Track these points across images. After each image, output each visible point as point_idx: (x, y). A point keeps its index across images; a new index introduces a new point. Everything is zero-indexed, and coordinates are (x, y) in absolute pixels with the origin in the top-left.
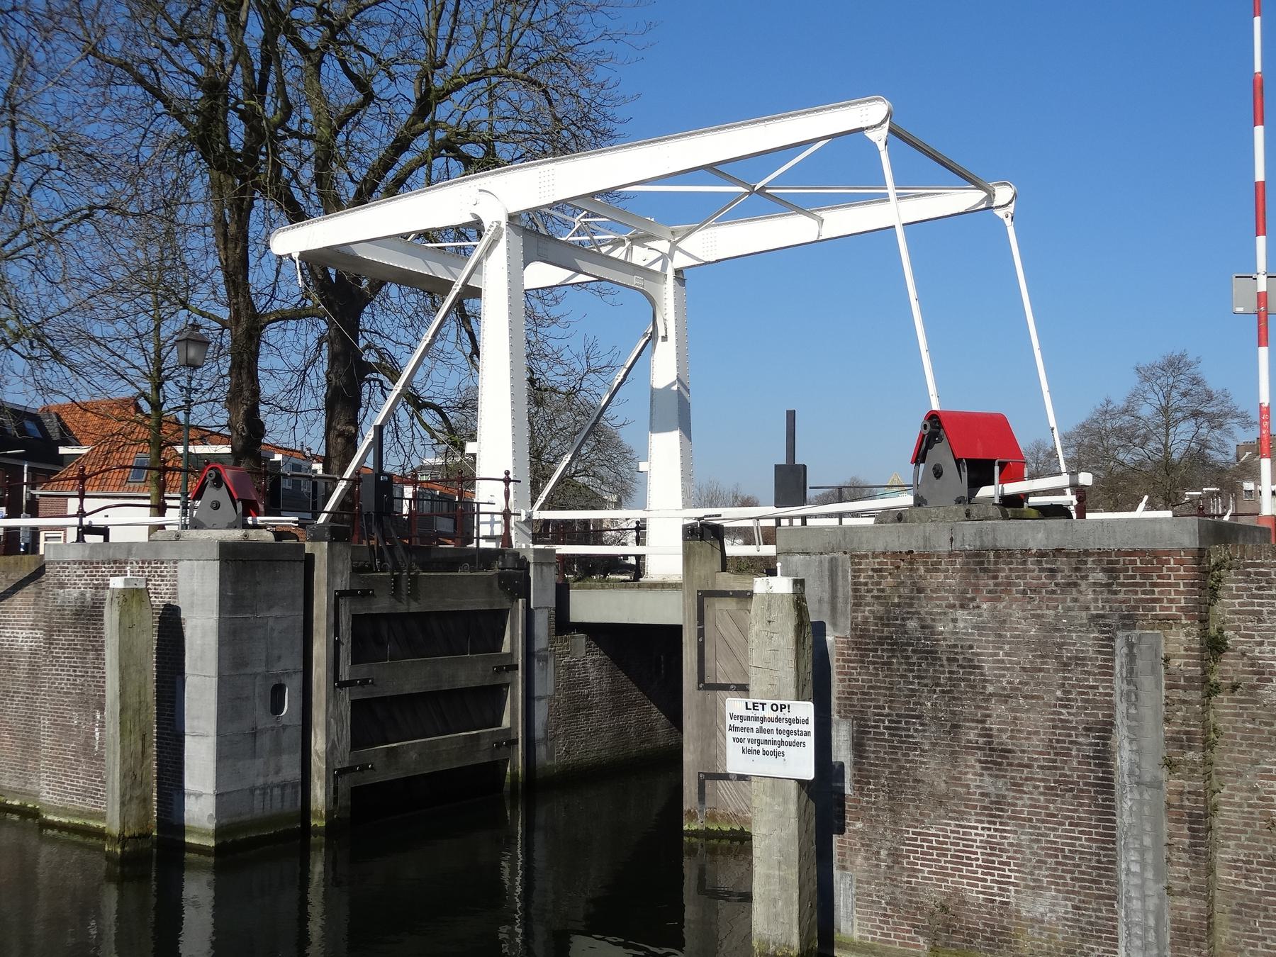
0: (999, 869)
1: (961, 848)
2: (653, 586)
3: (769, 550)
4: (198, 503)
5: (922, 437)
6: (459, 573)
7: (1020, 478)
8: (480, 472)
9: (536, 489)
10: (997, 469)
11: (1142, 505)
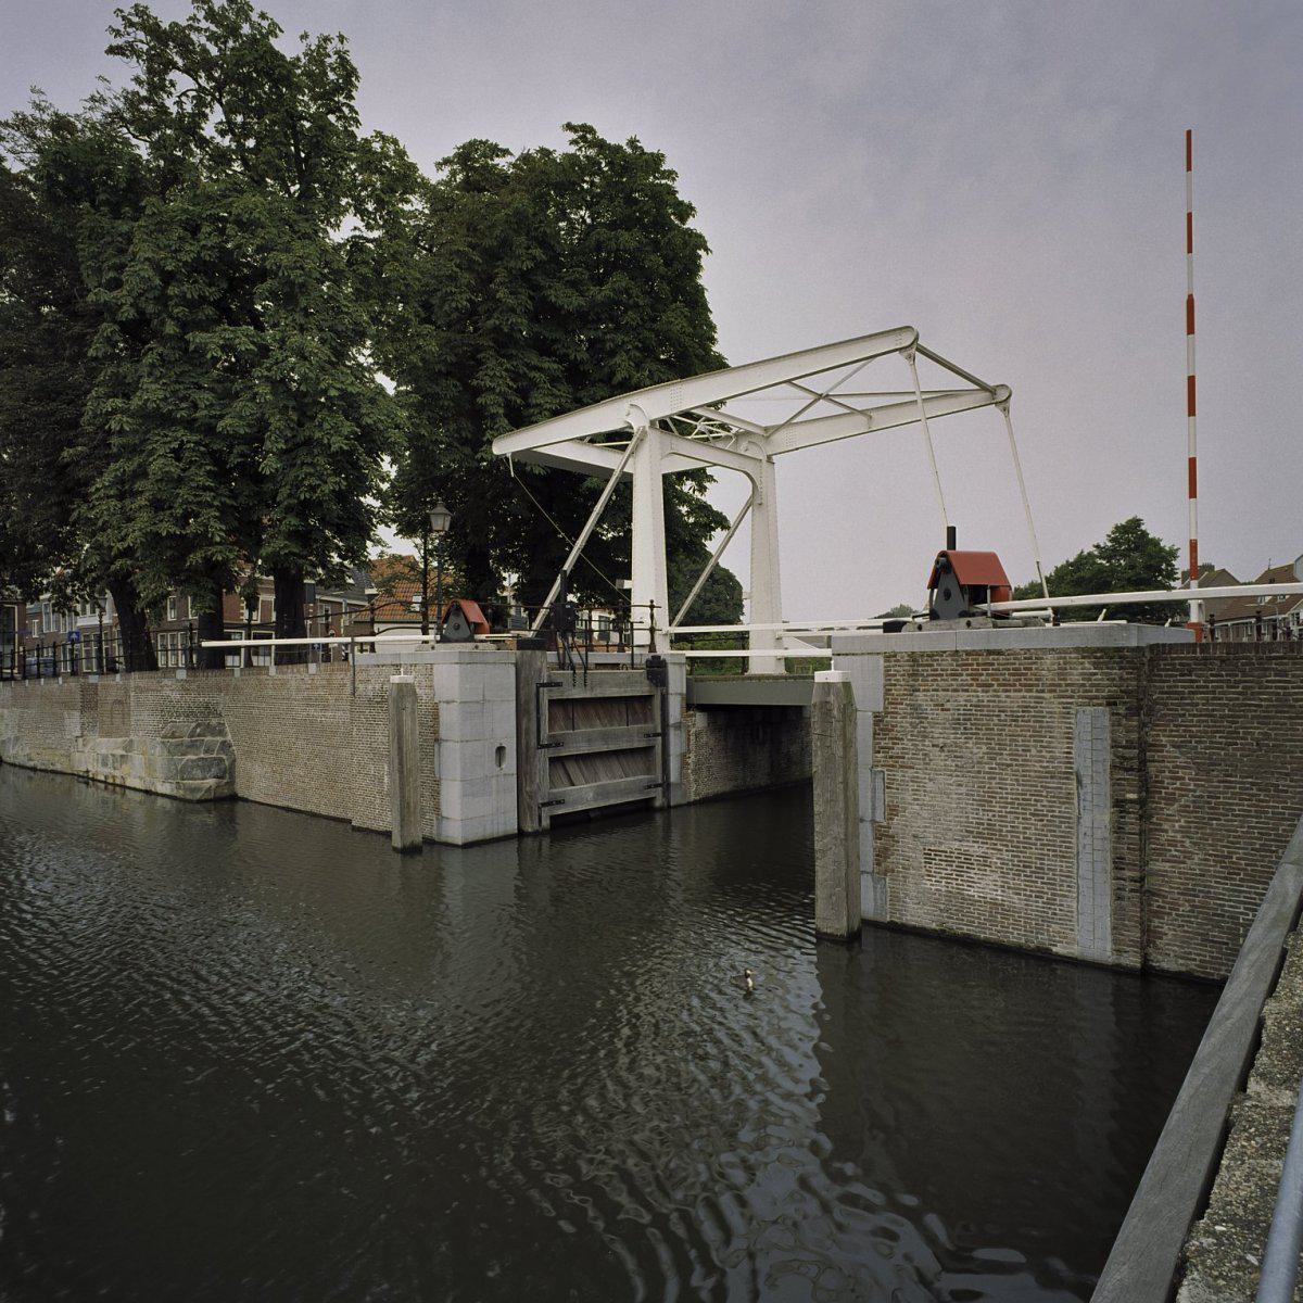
0: (1055, 836)
1: (963, 860)
2: (751, 678)
3: (827, 652)
4: (445, 626)
5: (1083, 561)
6: (902, 633)
7: (1006, 599)
8: (634, 601)
9: (673, 612)
10: (989, 592)
11: (1101, 616)
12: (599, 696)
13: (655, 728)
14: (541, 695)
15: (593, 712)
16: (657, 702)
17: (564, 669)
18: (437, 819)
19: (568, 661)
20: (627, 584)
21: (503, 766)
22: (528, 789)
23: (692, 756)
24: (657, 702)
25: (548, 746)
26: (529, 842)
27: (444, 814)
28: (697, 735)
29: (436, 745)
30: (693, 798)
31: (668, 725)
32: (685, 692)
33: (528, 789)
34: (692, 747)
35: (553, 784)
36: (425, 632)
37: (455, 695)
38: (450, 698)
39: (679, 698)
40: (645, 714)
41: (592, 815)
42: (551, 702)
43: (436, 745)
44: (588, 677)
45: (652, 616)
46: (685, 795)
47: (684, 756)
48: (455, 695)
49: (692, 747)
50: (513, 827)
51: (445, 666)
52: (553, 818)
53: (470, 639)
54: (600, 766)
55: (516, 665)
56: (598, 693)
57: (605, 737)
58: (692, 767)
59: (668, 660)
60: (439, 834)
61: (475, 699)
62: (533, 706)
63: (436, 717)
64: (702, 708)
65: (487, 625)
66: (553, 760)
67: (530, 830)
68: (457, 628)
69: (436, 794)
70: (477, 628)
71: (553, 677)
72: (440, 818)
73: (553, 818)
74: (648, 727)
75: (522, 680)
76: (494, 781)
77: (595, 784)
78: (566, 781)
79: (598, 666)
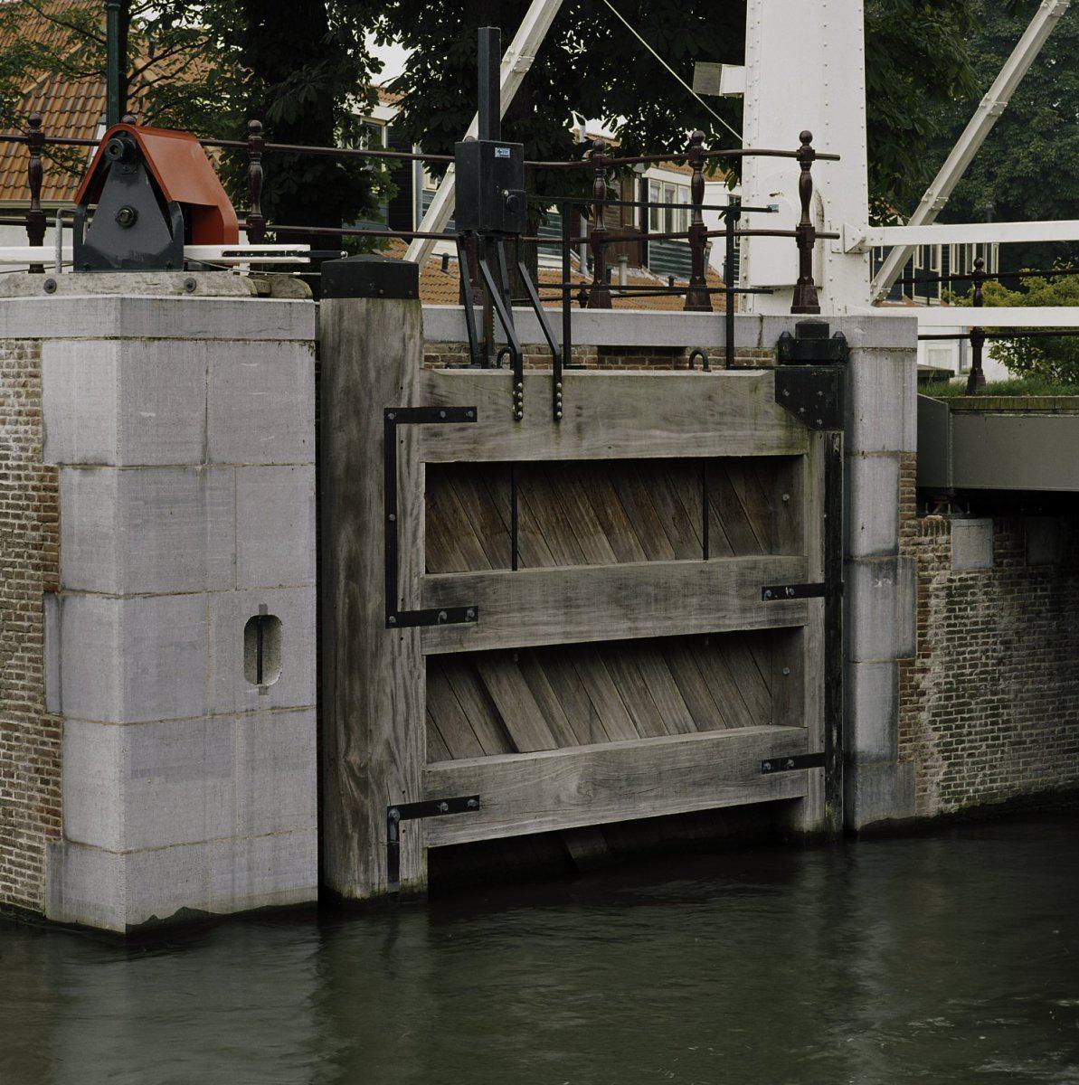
12: (605, 454)
13: (805, 571)
14: (401, 450)
15: (585, 511)
16: (811, 482)
17: (485, 365)
18: (53, 847)
19: (499, 337)
20: (730, 80)
21: (271, 681)
22: (354, 757)
23: (936, 665)
24: (811, 482)
25: (423, 619)
26: (359, 938)
27: (74, 832)
28: (955, 594)
29: (50, 607)
30: (933, 805)
31: (850, 560)
32: (912, 445)
33: (354, 757)
34: (937, 635)
35: (440, 744)
36: (36, 239)
37: (109, 444)
38: (90, 454)
39: (890, 469)
40: (768, 520)
41: (577, 851)
42: (439, 475)
43: (50, 607)
44: (568, 393)
45: (806, 190)
46: (907, 792)
47: (904, 667)
48: (109, 444)
49: (937, 635)
50: (301, 882)
51: (76, 346)
52: (438, 857)
53: (171, 260)
54: (610, 693)
55: (319, 348)
56: (600, 445)
57: (623, 595)
58: (932, 699)
59: (855, 336)
60: (59, 898)
61: (178, 457)
62: (372, 486)
63: (50, 514)
64: (976, 503)
65: (229, 213)
66: (439, 667)
67: (359, 893)
68: (130, 220)
69: (50, 768)
70: (200, 223)
71: (442, 390)
72: (64, 845)
73: (438, 857)
74: (780, 564)
75: (338, 393)
76: (239, 726)
77: (587, 749)
78: (485, 732)
79: (609, 354)
